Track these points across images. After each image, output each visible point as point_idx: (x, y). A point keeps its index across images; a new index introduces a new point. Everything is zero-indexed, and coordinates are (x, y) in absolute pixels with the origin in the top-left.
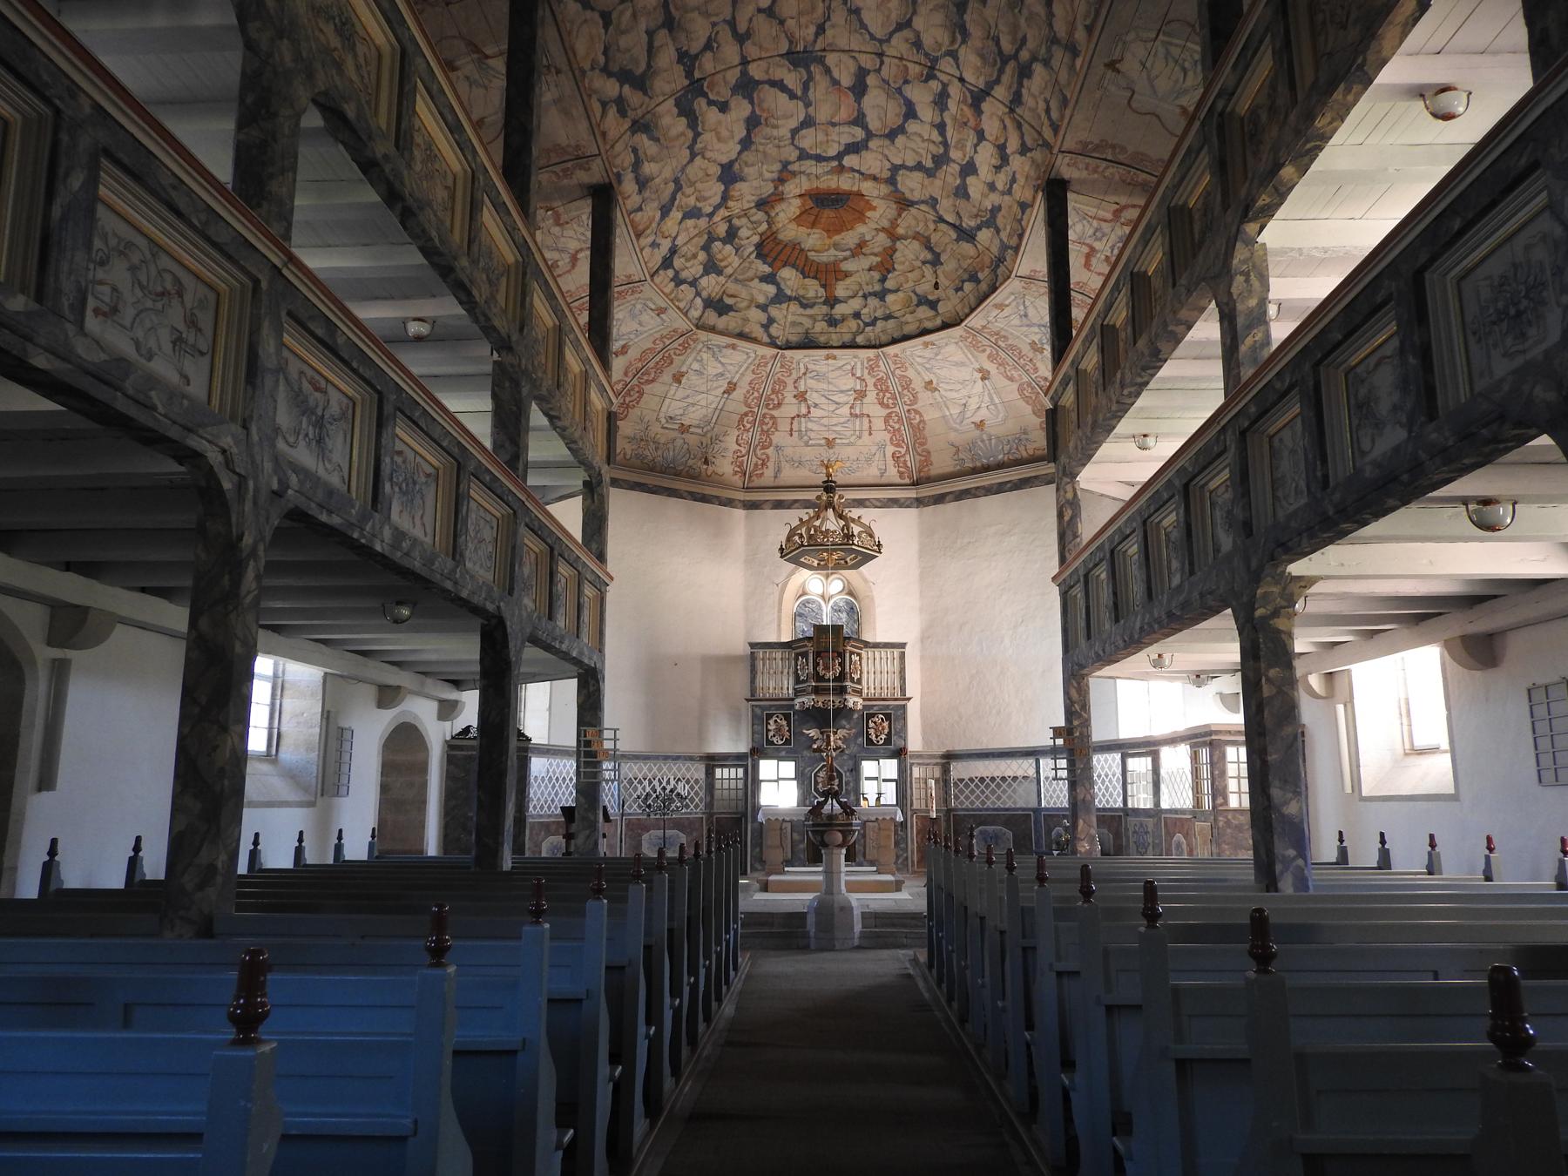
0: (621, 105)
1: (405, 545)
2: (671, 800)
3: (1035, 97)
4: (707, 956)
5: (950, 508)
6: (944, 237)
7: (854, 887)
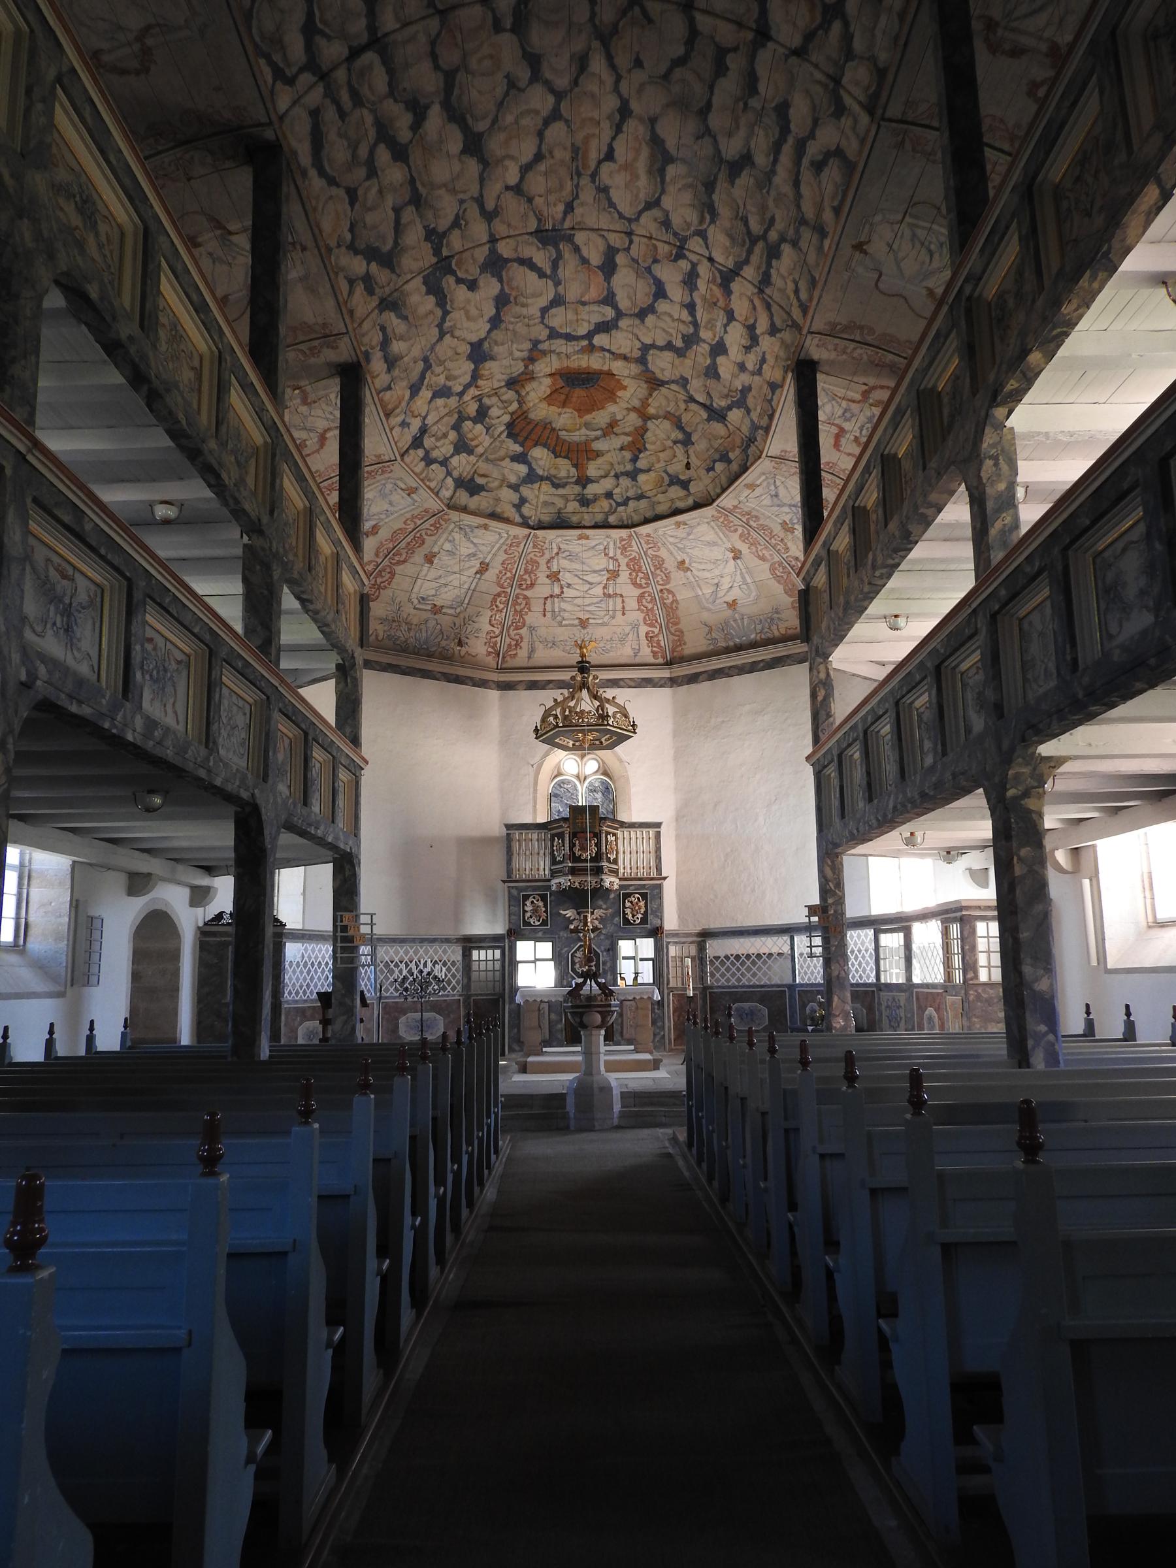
0: (368, 282)
1: (157, 734)
2: (429, 983)
3: (783, 278)
4: (470, 1143)
5: (704, 687)
6: (695, 417)
7: (613, 1067)
